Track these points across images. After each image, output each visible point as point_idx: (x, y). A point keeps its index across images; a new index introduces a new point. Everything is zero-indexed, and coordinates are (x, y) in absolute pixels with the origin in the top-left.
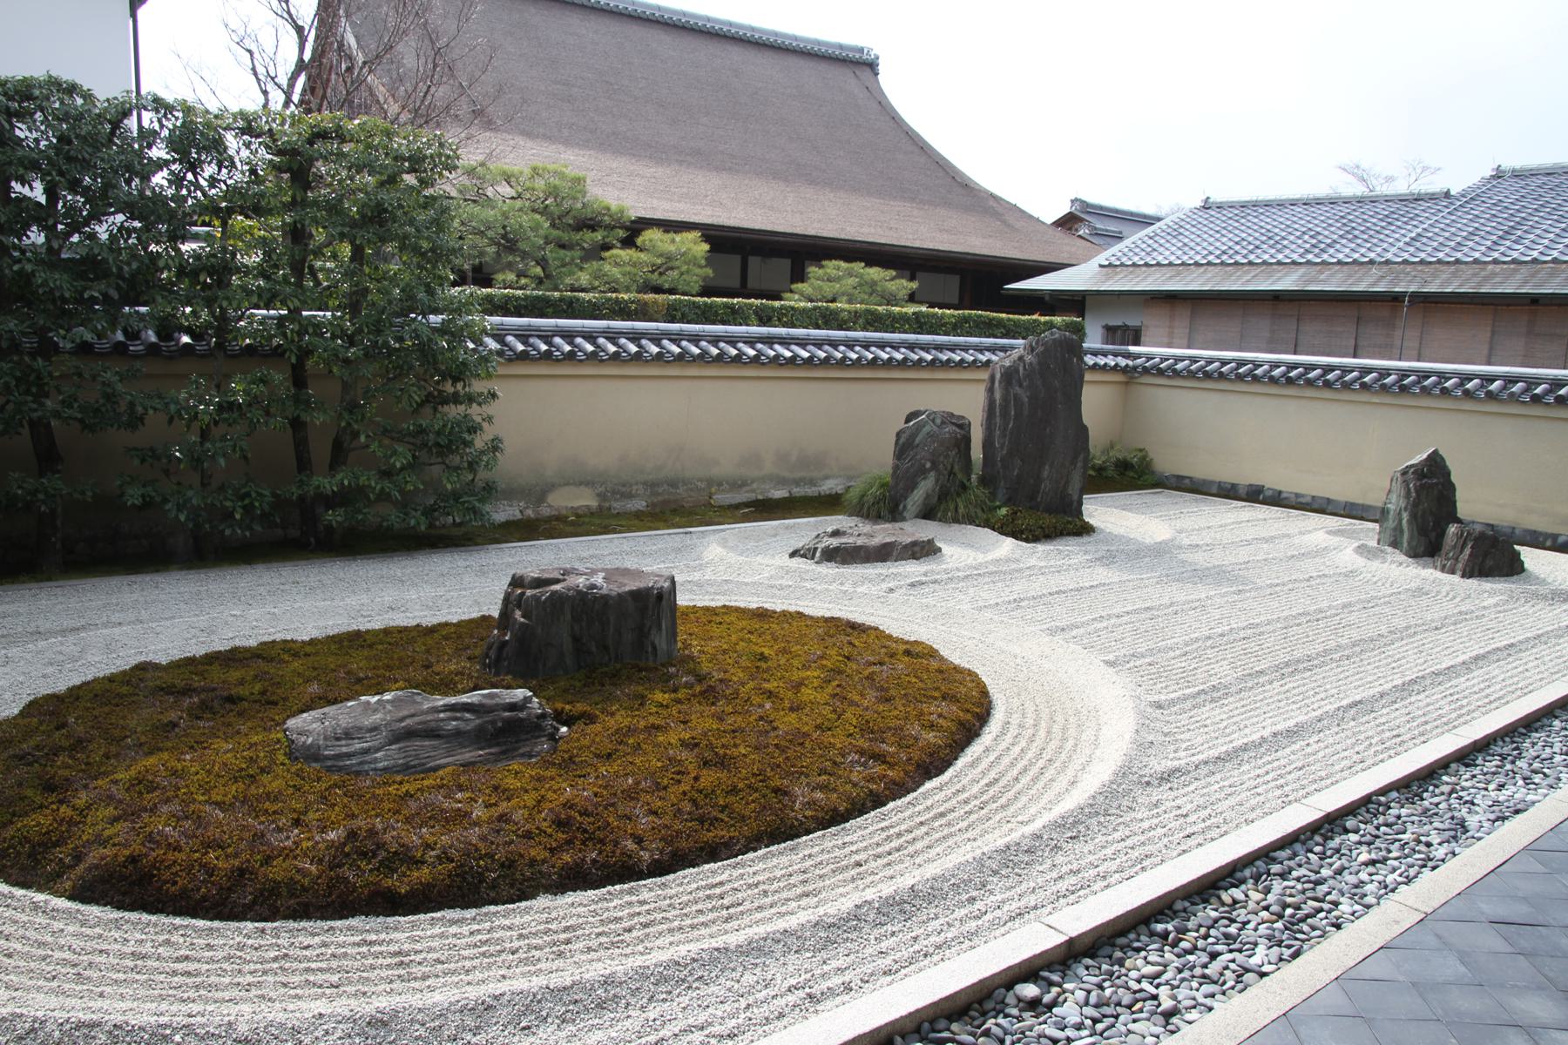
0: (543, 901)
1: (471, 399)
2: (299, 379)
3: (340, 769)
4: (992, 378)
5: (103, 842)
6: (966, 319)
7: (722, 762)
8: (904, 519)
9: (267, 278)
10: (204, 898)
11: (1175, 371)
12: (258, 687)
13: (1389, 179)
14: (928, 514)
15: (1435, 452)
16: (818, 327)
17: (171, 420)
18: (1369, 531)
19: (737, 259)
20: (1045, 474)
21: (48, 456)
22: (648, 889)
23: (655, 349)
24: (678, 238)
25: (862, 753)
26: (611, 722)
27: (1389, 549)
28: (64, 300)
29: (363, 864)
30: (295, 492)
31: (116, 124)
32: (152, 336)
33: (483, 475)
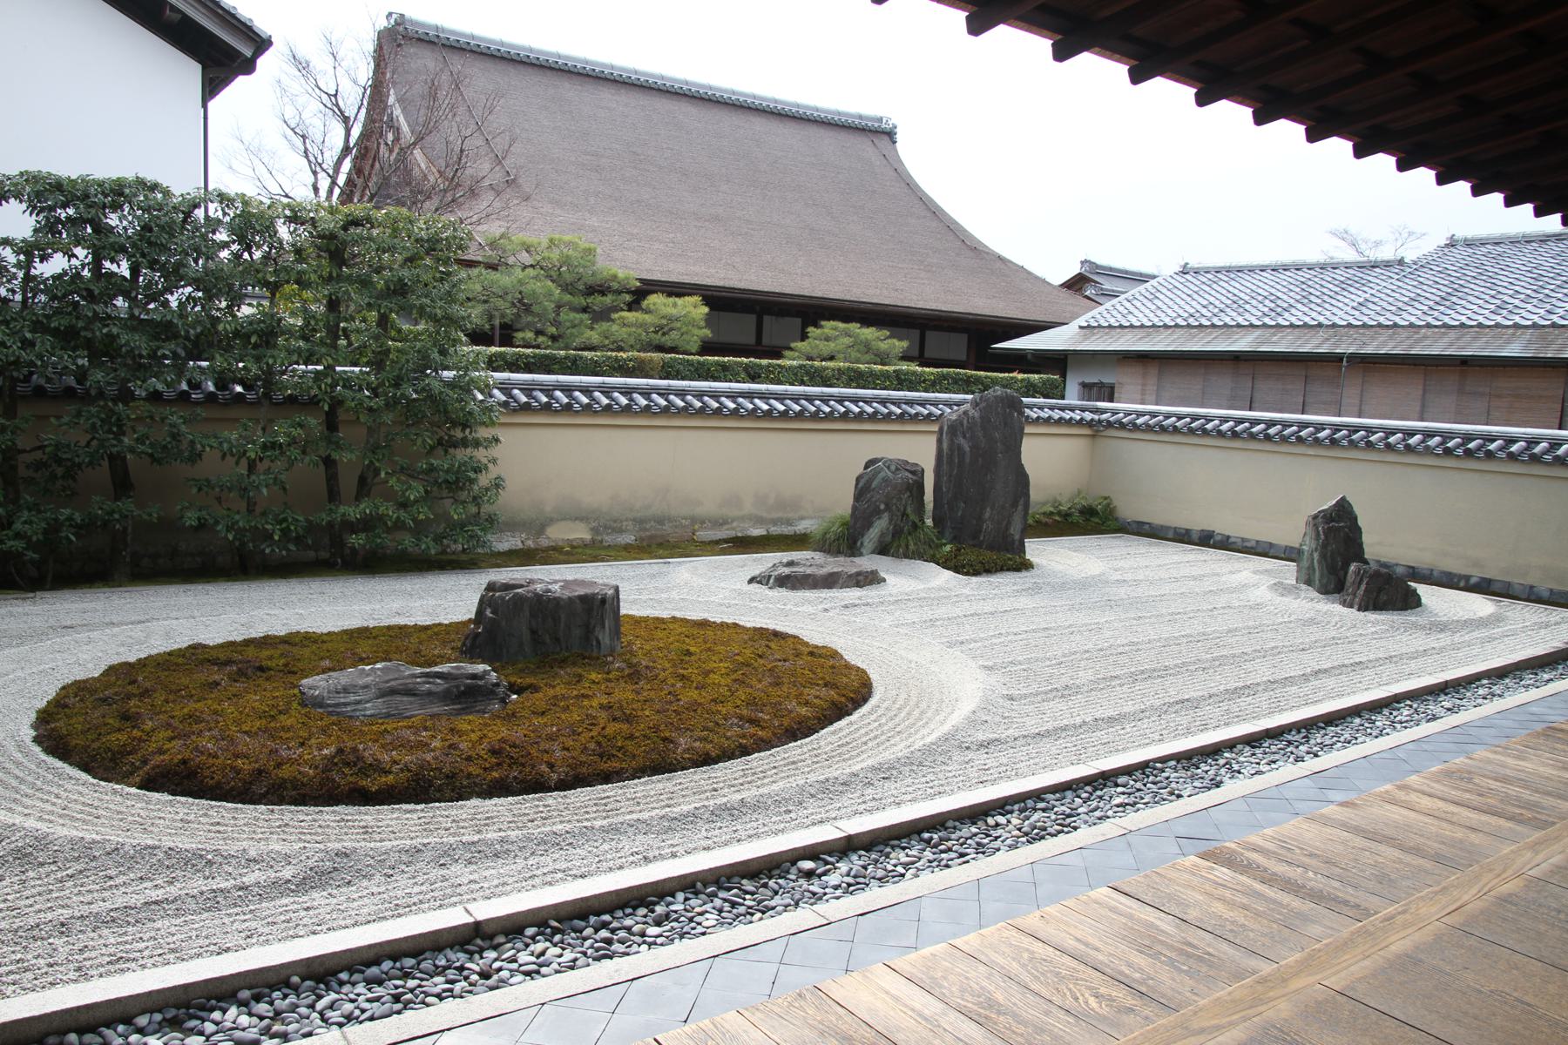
0: (475, 802)
1: (477, 444)
2: (331, 424)
3: (338, 714)
4: (941, 429)
5: (161, 751)
6: (944, 377)
7: (628, 719)
8: (861, 555)
9: (305, 338)
10: (232, 789)
11: (1135, 425)
12: (282, 661)
13: (1378, 244)
14: (883, 550)
15: (1343, 499)
16: (802, 383)
17: (224, 456)
18: (1289, 571)
19: (753, 318)
20: (987, 515)
21: (122, 484)
22: (553, 799)
23: (643, 402)
24: (680, 301)
25: (741, 718)
26: (551, 692)
27: (1304, 587)
28: (141, 356)
29: (346, 770)
30: (324, 518)
31: (188, 215)
32: (211, 387)
33: (486, 509)
